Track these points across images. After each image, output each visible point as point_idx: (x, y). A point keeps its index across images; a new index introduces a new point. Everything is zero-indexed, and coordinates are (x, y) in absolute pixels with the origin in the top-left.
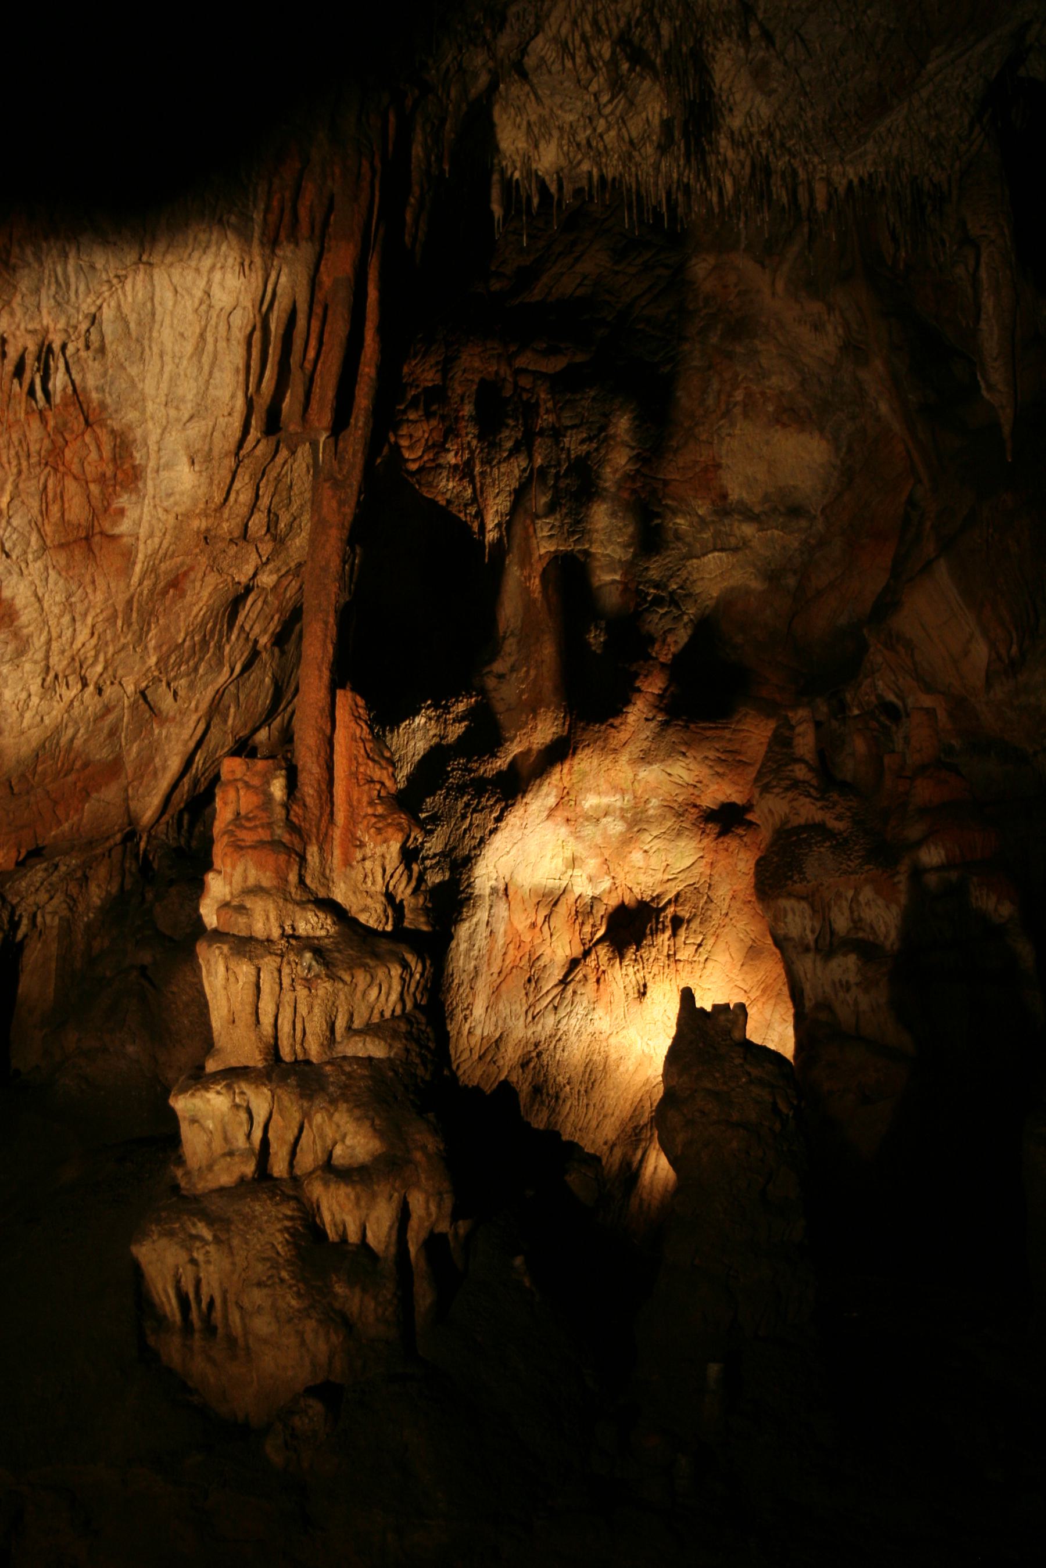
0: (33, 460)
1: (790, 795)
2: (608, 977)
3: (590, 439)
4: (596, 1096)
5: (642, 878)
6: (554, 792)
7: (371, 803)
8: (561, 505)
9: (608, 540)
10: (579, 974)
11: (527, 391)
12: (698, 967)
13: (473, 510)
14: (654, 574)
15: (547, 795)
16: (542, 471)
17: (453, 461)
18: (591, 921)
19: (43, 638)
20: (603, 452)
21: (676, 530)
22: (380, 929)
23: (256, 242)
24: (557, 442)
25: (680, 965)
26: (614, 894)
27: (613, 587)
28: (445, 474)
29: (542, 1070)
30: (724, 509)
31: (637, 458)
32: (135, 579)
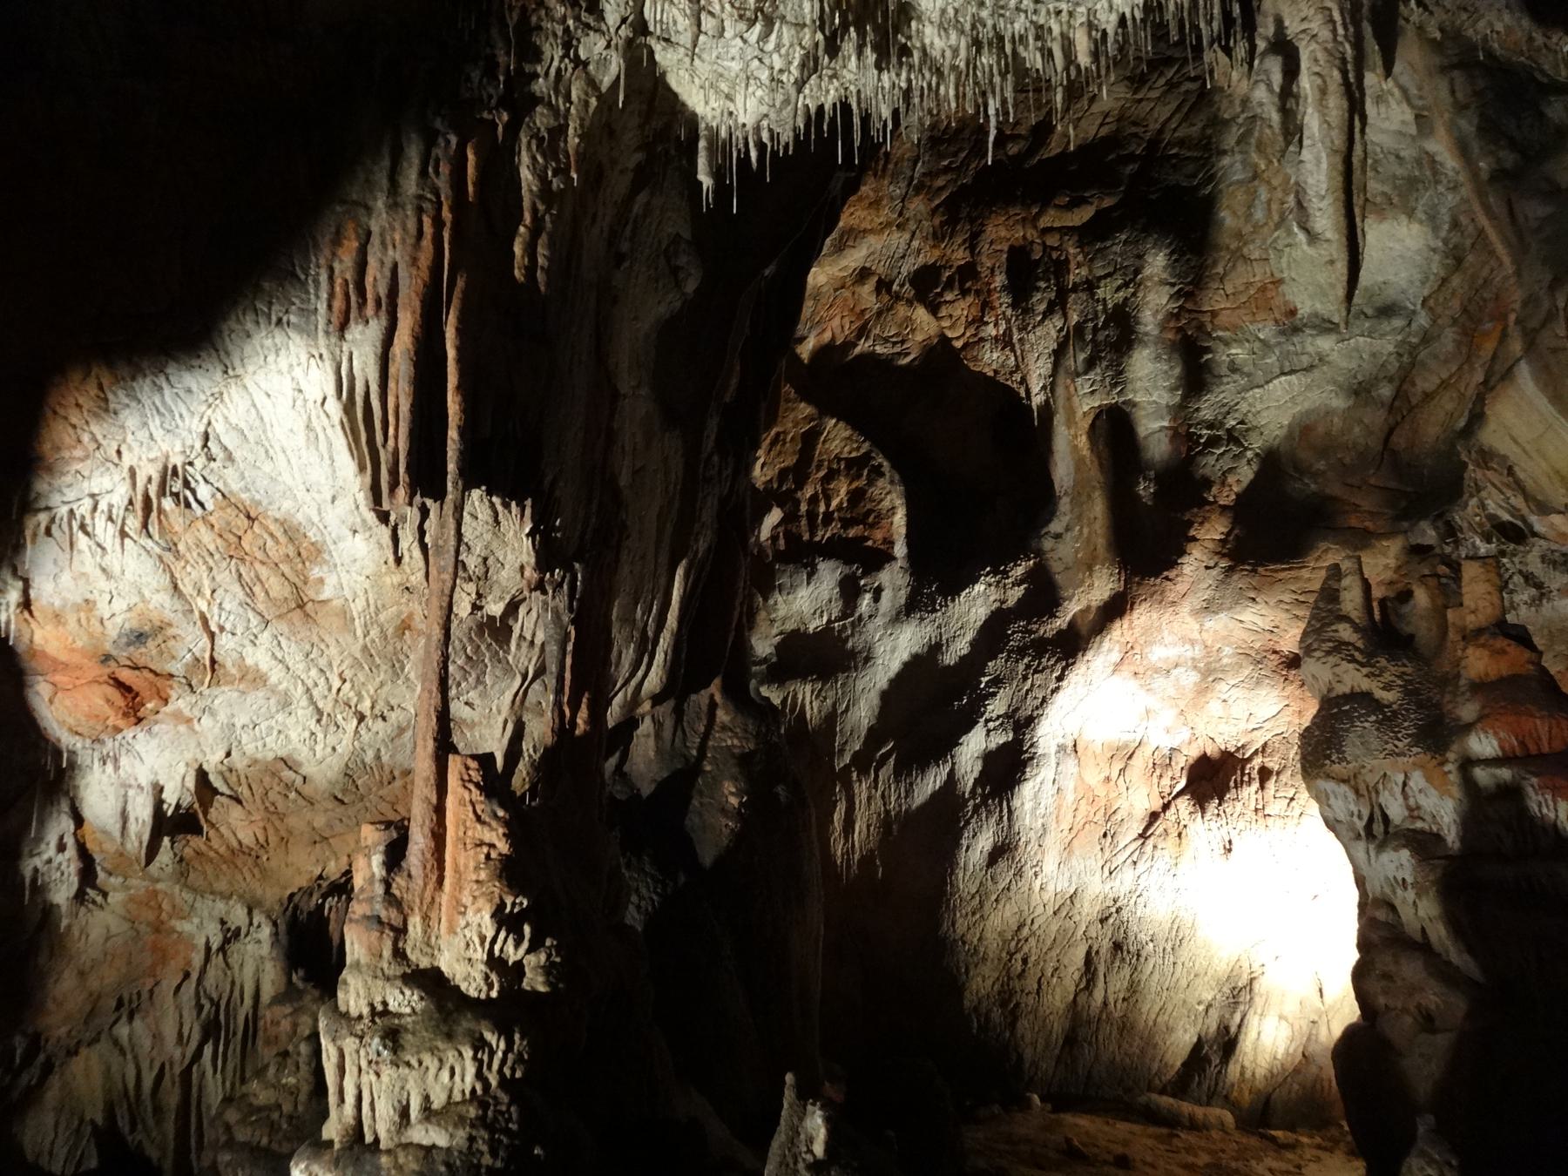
0: (217, 556)
1: (1332, 659)
2: (1190, 831)
3: (1126, 285)
4: (1184, 954)
5: (1223, 728)
6: (1117, 648)
7: (477, 868)
8: (1101, 359)
9: (1150, 382)
10: (1159, 827)
11: (1056, 249)
12: (1291, 823)
13: (1017, 377)
14: (1207, 413)
15: (1110, 650)
16: (1079, 328)
17: (994, 333)
18: (1170, 774)
19: (300, 689)
20: (1140, 295)
21: (1232, 361)
22: (483, 996)
23: (321, 334)
24: (1092, 295)
25: (1270, 821)
26: (1194, 745)
27: (1162, 435)
28: (988, 346)
29: (1122, 926)
30: (1291, 325)
31: (1177, 295)
32: (359, 632)
